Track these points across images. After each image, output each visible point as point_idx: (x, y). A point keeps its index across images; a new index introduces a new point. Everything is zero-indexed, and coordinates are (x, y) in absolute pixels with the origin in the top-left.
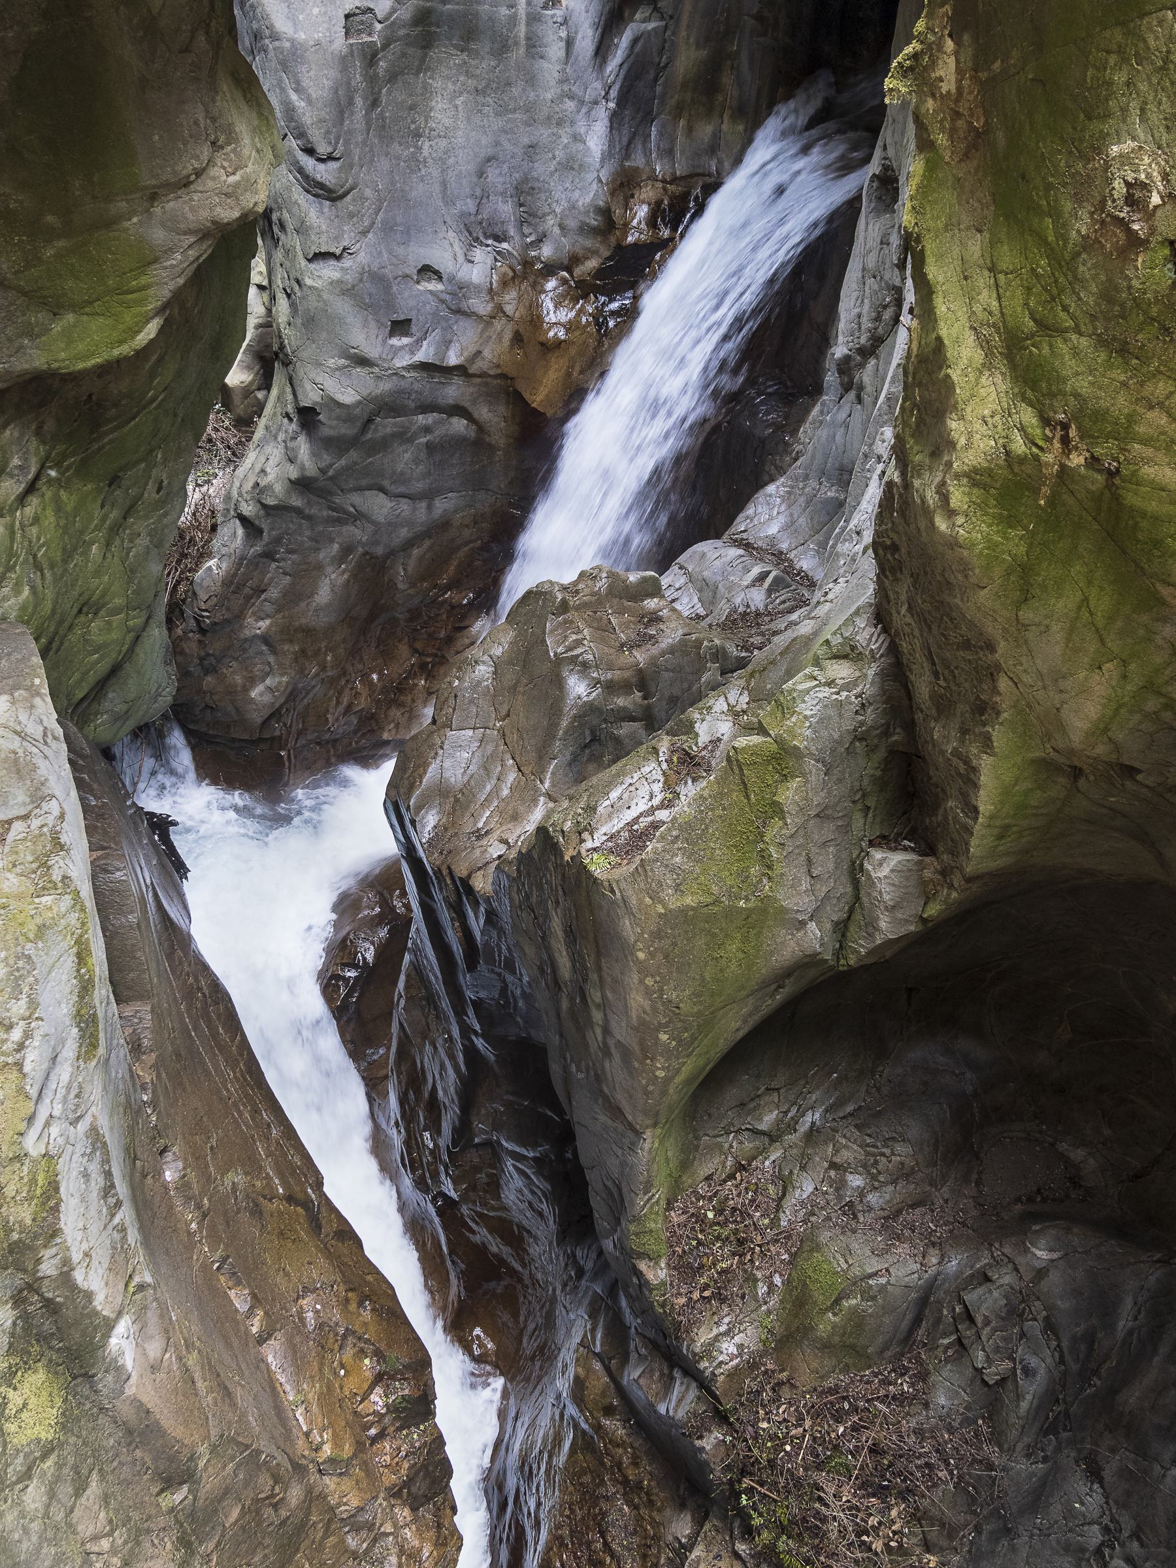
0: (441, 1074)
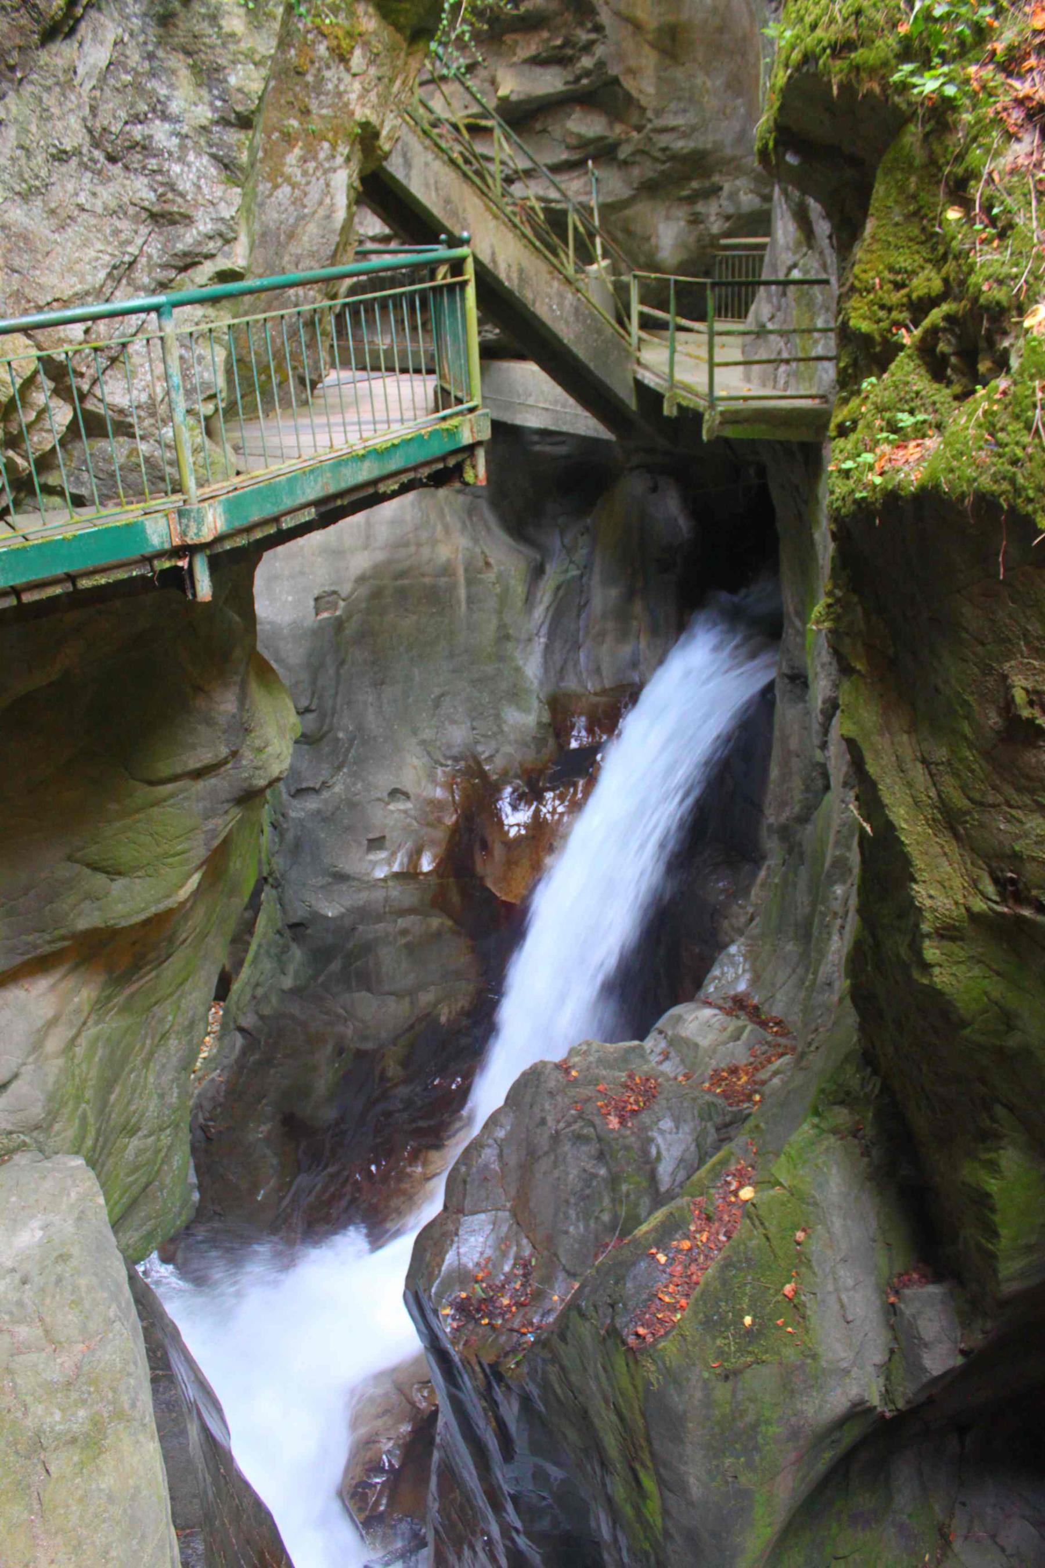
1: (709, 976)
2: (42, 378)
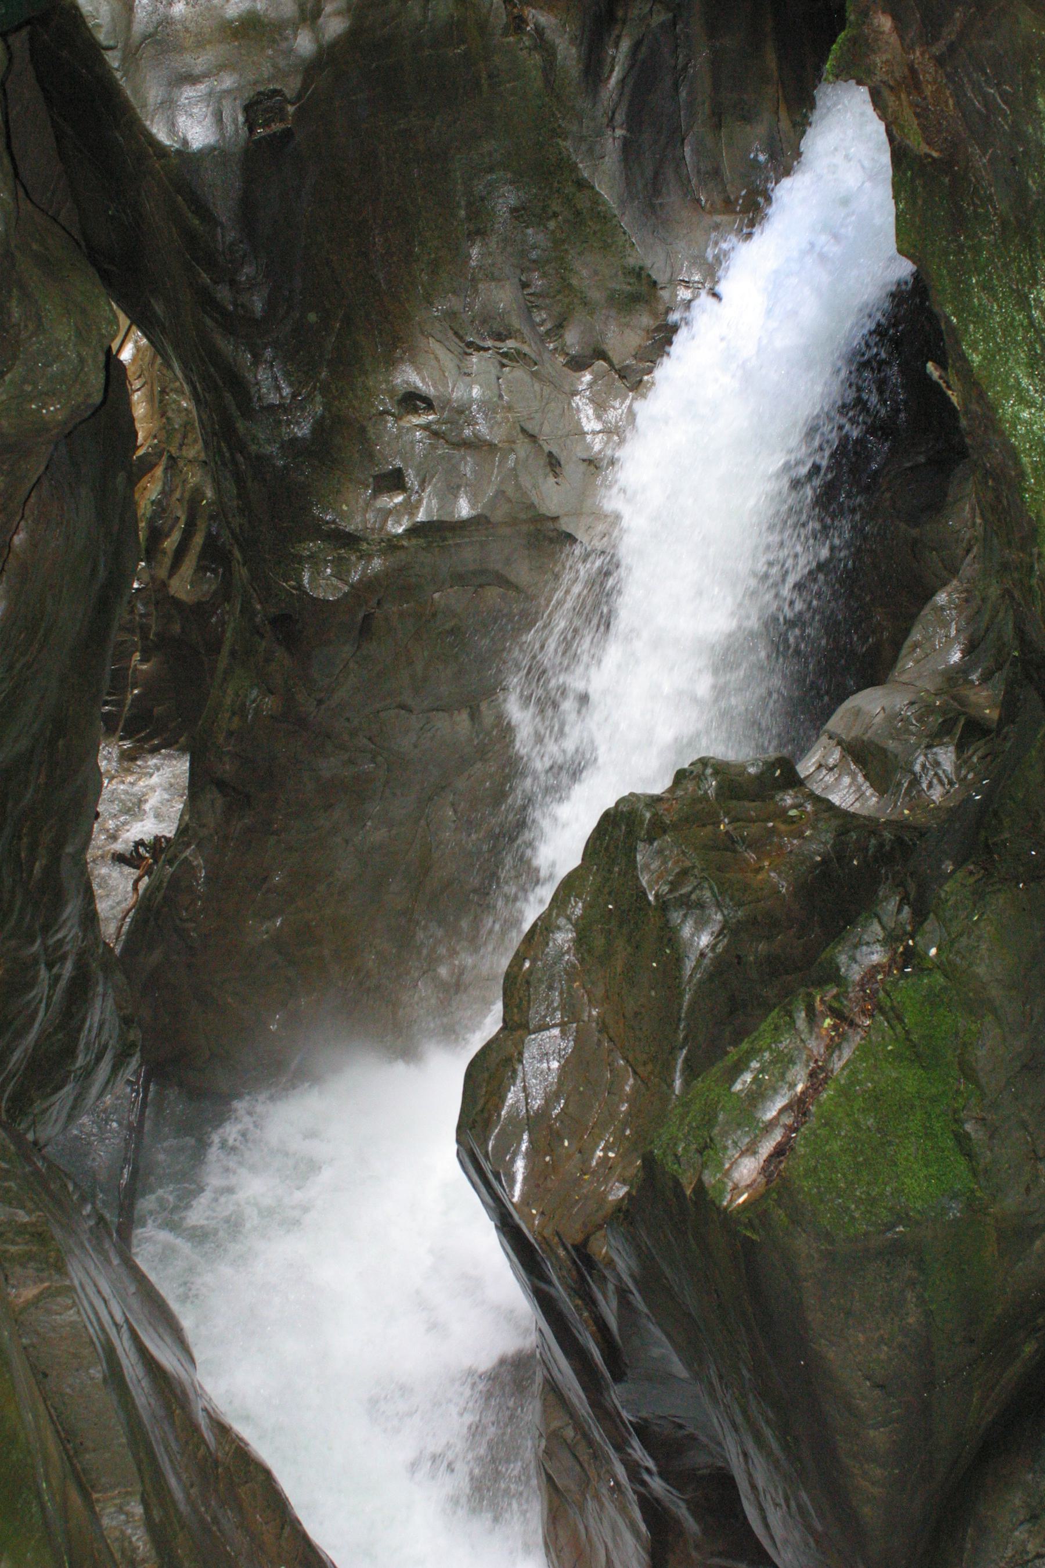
0: (614, 1540)
1: (908, 643)
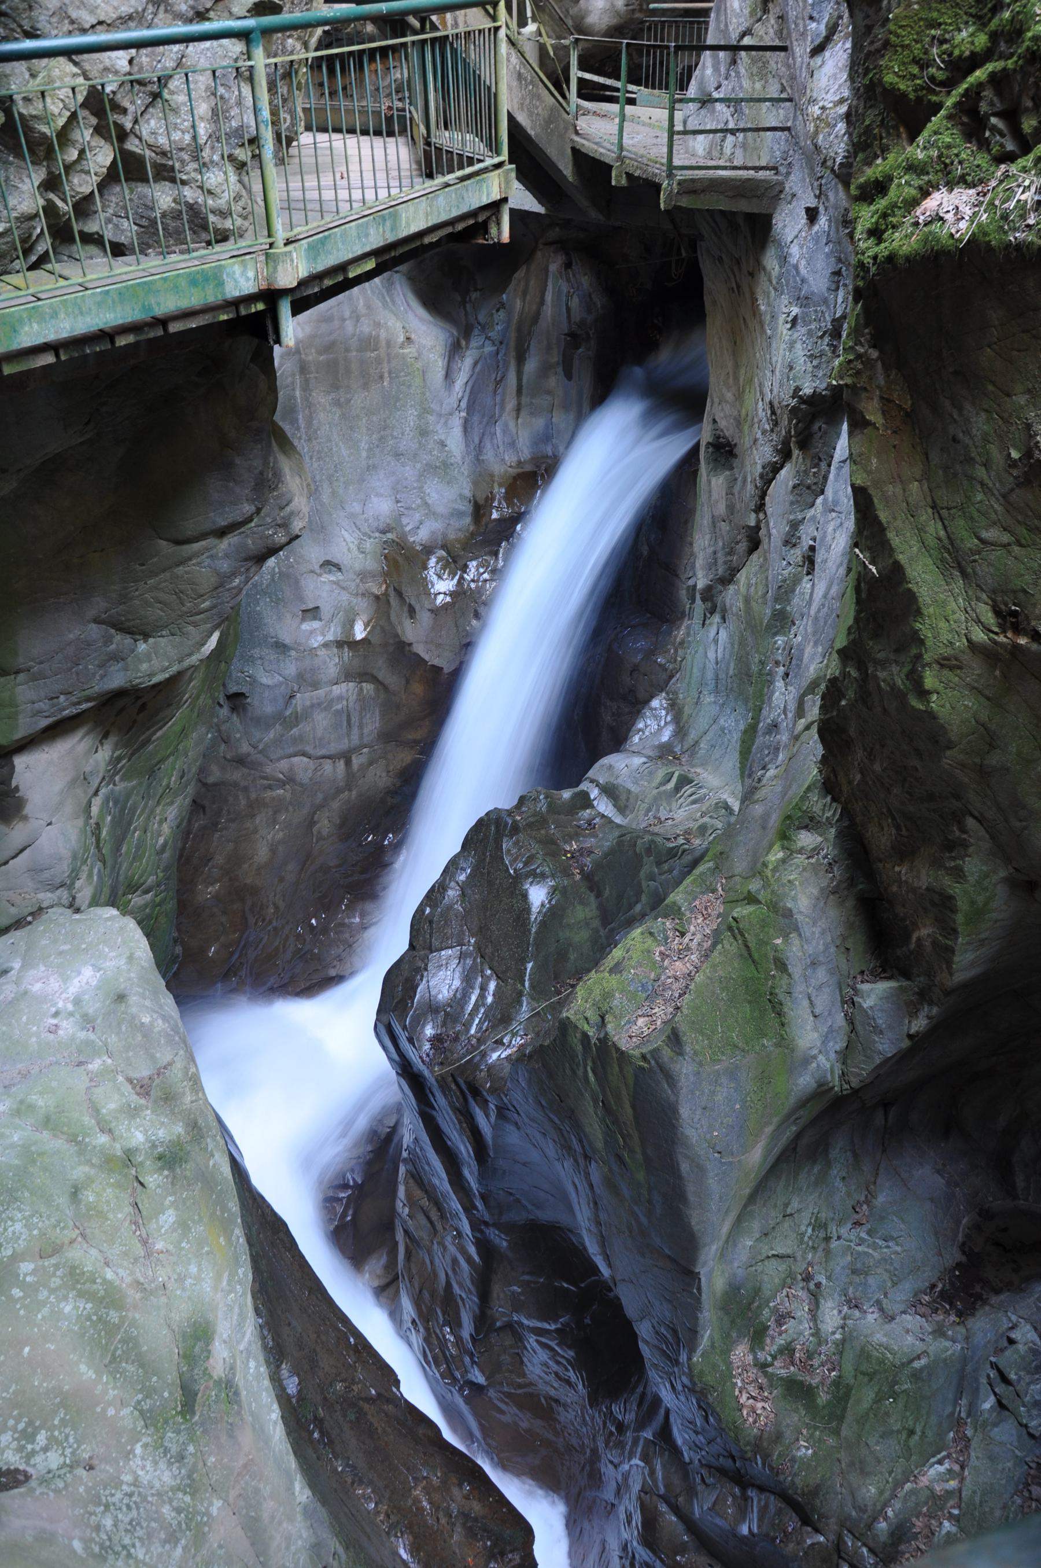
0: (454, 1270)
2: (82, 113)
